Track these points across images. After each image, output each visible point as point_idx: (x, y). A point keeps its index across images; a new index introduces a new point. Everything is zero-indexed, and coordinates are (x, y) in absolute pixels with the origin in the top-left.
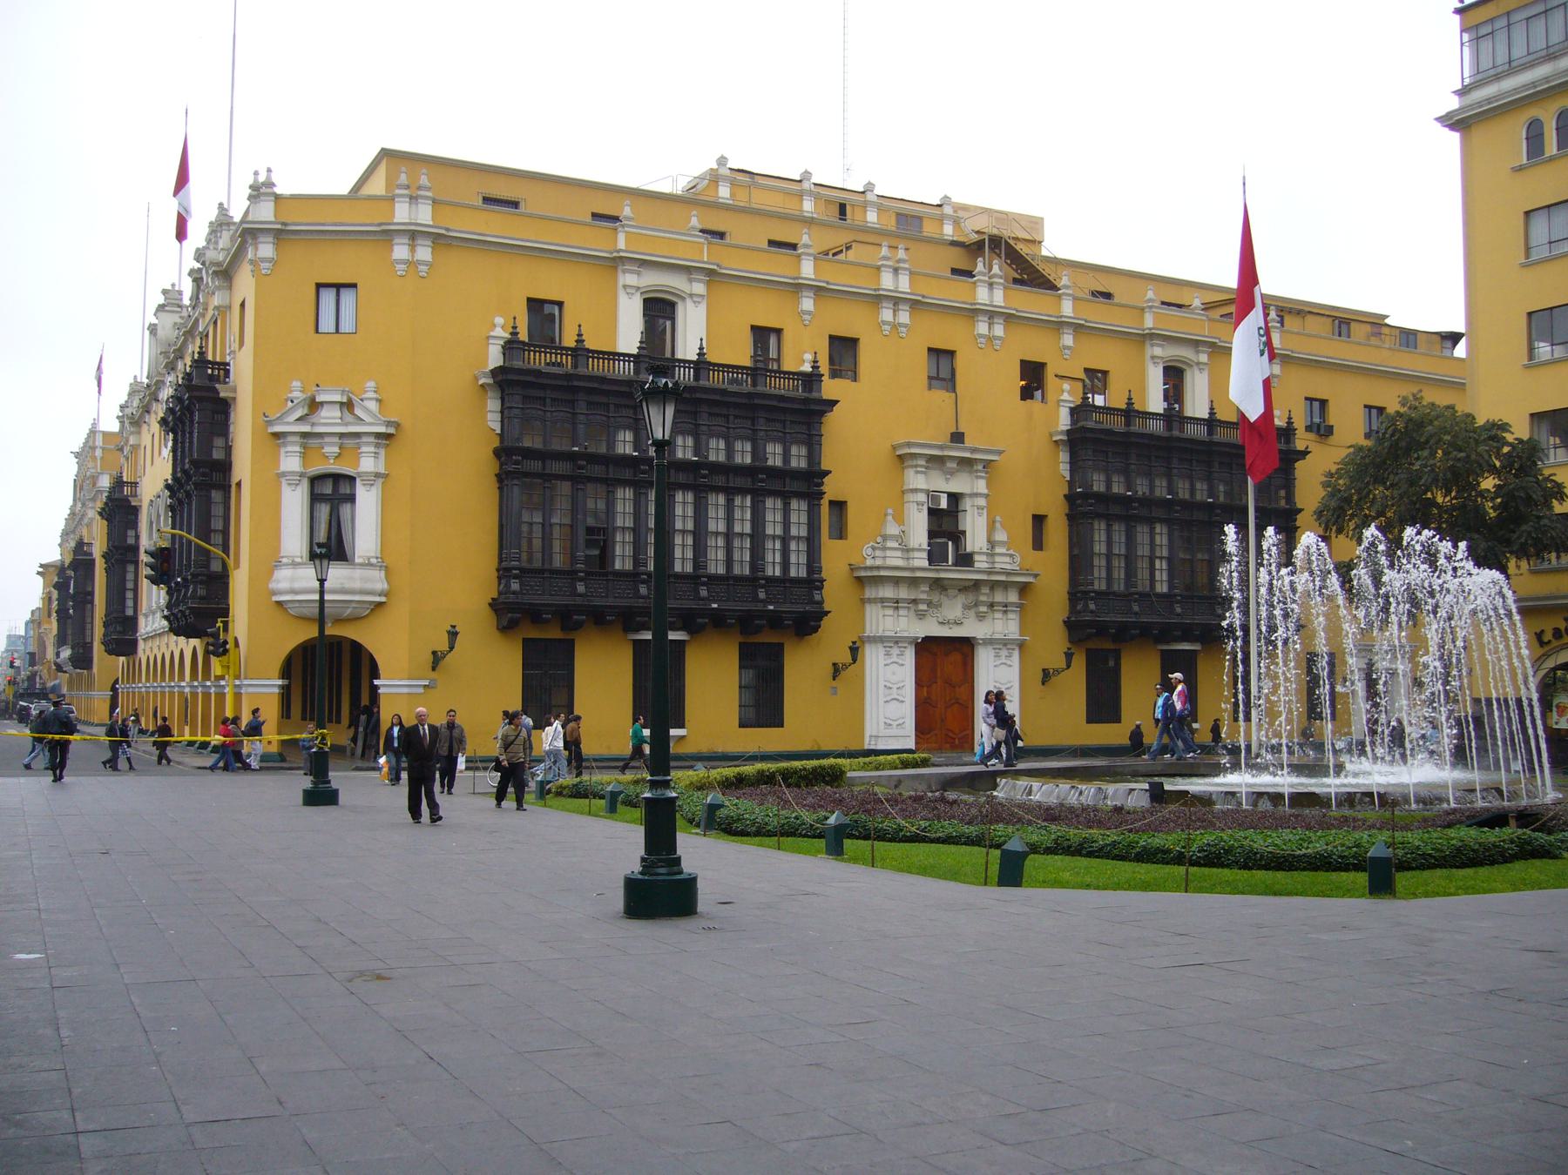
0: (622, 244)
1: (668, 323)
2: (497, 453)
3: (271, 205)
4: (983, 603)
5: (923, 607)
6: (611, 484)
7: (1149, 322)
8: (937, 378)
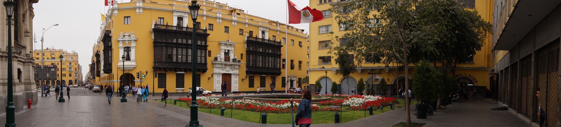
0: (174, 8)
1: (182, 21)
2: (153, 42)
3: (117, 5)
5: (223, 68)
6: (172, 48)
7: (260, 24)
8: (226, 31)
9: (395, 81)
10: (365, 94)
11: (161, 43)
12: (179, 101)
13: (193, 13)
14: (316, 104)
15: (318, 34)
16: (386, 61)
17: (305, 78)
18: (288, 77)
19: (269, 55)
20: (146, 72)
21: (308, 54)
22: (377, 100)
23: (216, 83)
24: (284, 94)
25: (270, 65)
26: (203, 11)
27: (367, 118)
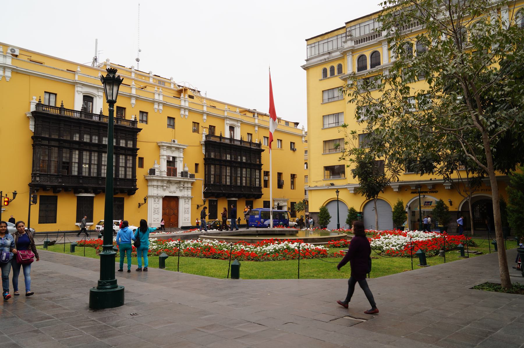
0: (77, 78)
1: (91, 103)
2: (33, 138)
4: (182, 187)
6: (71, 150)
7: (226, 114)
8: (170, 125)
9: (465, 205)
10: (408, 229)
11: (49, 140)
12: (80, 246)
13: (110, 89)
14: (322, 245)
15: (322, 129)
16: (444, 170)
17: (302, 202)
18: (274, 201)
19: (242, 165)
20: (13, 193)
21: (306, 163)
22: (432, 239)
23: (153, 213)
24: (268, 229)
25: (244, 181)
26: (131, 88)
27: (414, 271)
